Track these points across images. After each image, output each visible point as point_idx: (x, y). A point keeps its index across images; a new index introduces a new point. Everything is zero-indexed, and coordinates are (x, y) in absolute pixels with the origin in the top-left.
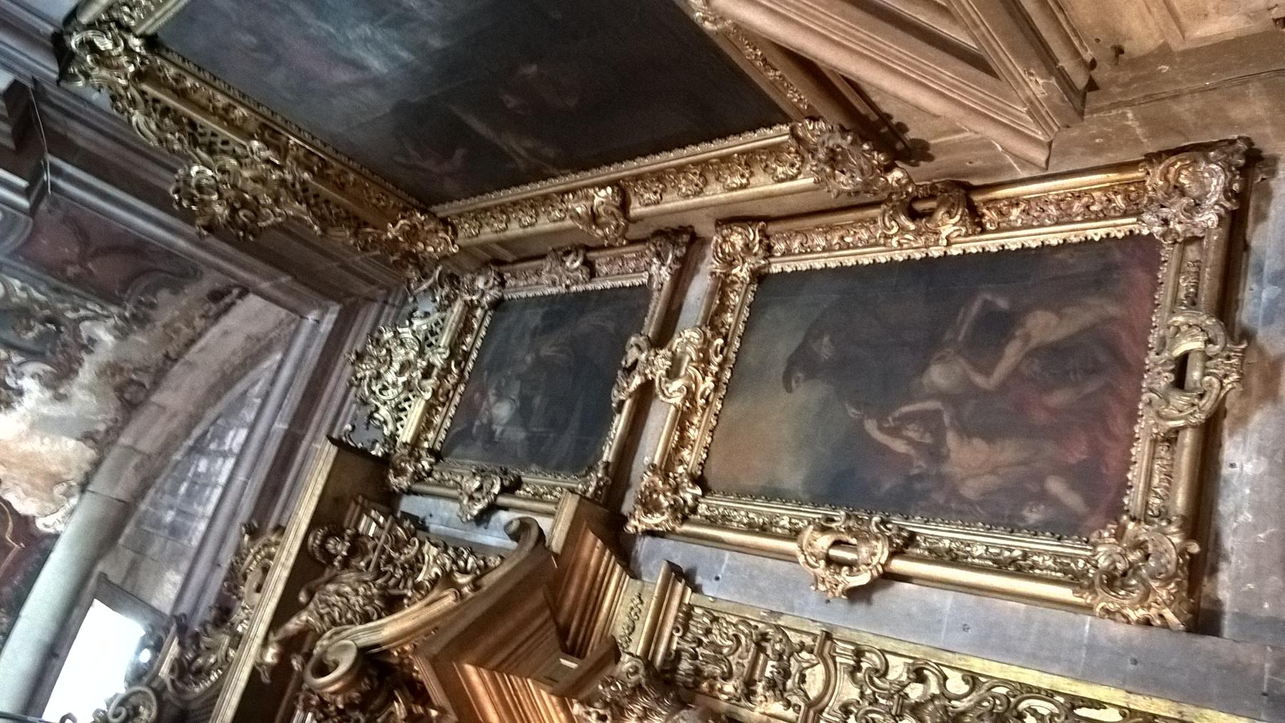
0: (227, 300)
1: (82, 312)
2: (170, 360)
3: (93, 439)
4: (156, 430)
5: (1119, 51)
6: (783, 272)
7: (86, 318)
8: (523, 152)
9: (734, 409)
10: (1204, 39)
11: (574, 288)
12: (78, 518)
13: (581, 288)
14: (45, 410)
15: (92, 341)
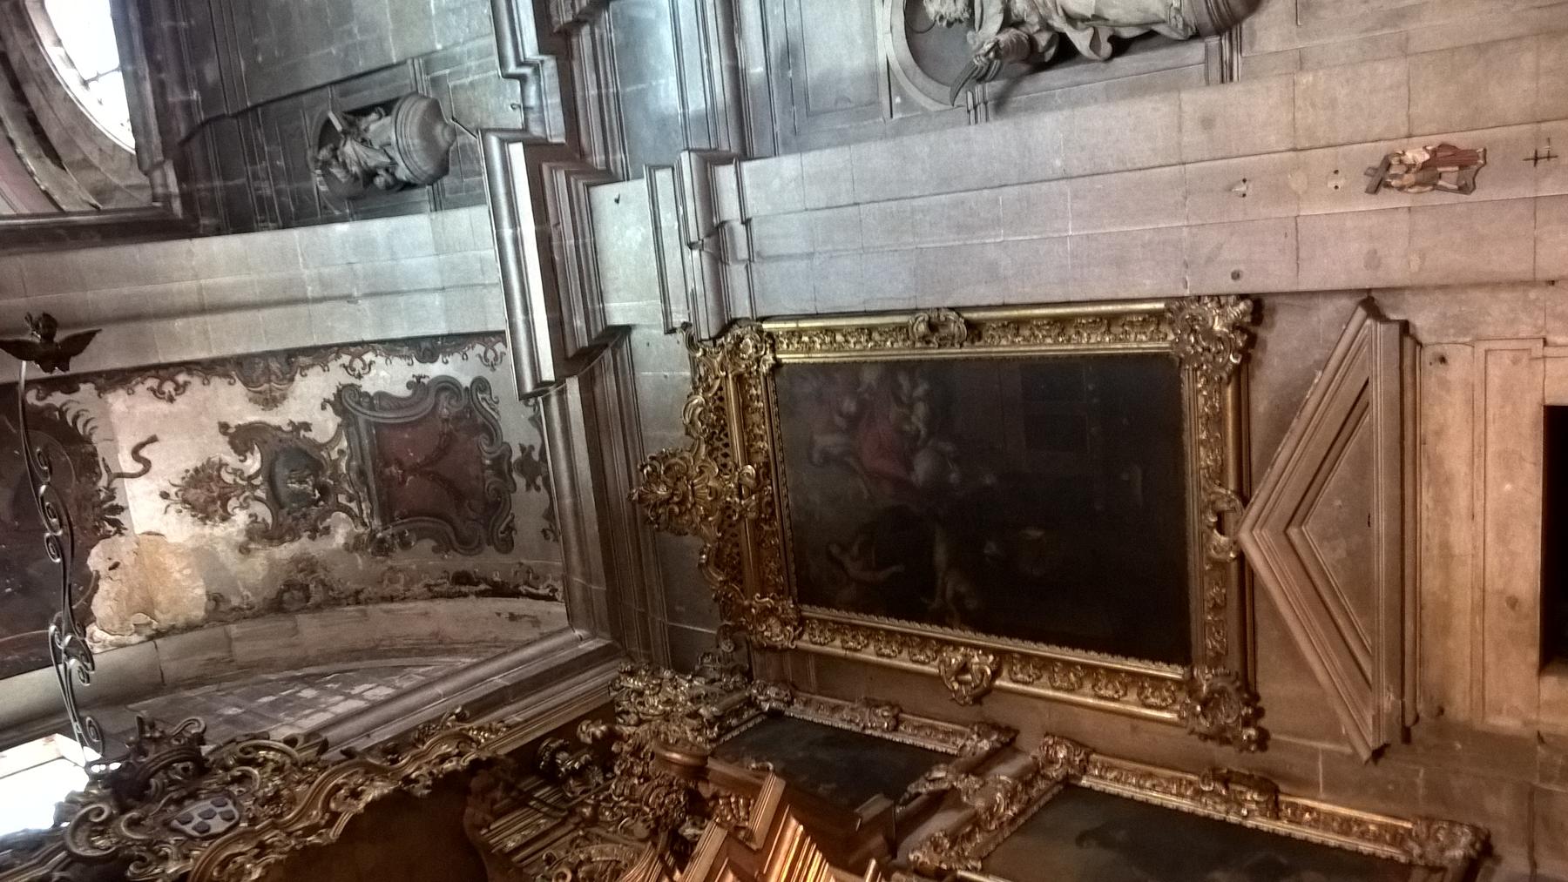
0: (464, 589)
1: (353, 505)
2: (356, 598)
3: (217, 604)
4: (263, 645)
5: (1441, 711)
6: (1090, 789)
7: (348, 511)
8: (949, 593)
9: (1017, 840)
10: (1494, 726)
11: (868, 732)
12: (119, 656)
13: (877, 734)
14: (220, 547)
15: (327, 530)
